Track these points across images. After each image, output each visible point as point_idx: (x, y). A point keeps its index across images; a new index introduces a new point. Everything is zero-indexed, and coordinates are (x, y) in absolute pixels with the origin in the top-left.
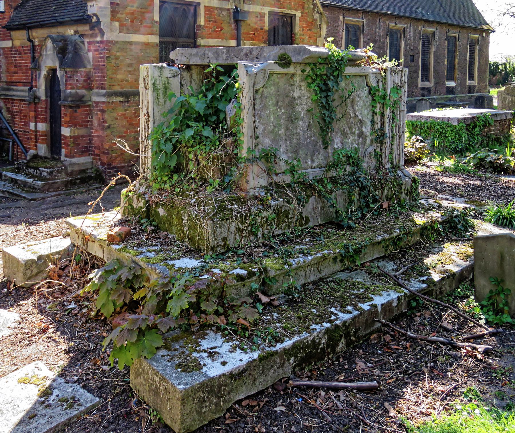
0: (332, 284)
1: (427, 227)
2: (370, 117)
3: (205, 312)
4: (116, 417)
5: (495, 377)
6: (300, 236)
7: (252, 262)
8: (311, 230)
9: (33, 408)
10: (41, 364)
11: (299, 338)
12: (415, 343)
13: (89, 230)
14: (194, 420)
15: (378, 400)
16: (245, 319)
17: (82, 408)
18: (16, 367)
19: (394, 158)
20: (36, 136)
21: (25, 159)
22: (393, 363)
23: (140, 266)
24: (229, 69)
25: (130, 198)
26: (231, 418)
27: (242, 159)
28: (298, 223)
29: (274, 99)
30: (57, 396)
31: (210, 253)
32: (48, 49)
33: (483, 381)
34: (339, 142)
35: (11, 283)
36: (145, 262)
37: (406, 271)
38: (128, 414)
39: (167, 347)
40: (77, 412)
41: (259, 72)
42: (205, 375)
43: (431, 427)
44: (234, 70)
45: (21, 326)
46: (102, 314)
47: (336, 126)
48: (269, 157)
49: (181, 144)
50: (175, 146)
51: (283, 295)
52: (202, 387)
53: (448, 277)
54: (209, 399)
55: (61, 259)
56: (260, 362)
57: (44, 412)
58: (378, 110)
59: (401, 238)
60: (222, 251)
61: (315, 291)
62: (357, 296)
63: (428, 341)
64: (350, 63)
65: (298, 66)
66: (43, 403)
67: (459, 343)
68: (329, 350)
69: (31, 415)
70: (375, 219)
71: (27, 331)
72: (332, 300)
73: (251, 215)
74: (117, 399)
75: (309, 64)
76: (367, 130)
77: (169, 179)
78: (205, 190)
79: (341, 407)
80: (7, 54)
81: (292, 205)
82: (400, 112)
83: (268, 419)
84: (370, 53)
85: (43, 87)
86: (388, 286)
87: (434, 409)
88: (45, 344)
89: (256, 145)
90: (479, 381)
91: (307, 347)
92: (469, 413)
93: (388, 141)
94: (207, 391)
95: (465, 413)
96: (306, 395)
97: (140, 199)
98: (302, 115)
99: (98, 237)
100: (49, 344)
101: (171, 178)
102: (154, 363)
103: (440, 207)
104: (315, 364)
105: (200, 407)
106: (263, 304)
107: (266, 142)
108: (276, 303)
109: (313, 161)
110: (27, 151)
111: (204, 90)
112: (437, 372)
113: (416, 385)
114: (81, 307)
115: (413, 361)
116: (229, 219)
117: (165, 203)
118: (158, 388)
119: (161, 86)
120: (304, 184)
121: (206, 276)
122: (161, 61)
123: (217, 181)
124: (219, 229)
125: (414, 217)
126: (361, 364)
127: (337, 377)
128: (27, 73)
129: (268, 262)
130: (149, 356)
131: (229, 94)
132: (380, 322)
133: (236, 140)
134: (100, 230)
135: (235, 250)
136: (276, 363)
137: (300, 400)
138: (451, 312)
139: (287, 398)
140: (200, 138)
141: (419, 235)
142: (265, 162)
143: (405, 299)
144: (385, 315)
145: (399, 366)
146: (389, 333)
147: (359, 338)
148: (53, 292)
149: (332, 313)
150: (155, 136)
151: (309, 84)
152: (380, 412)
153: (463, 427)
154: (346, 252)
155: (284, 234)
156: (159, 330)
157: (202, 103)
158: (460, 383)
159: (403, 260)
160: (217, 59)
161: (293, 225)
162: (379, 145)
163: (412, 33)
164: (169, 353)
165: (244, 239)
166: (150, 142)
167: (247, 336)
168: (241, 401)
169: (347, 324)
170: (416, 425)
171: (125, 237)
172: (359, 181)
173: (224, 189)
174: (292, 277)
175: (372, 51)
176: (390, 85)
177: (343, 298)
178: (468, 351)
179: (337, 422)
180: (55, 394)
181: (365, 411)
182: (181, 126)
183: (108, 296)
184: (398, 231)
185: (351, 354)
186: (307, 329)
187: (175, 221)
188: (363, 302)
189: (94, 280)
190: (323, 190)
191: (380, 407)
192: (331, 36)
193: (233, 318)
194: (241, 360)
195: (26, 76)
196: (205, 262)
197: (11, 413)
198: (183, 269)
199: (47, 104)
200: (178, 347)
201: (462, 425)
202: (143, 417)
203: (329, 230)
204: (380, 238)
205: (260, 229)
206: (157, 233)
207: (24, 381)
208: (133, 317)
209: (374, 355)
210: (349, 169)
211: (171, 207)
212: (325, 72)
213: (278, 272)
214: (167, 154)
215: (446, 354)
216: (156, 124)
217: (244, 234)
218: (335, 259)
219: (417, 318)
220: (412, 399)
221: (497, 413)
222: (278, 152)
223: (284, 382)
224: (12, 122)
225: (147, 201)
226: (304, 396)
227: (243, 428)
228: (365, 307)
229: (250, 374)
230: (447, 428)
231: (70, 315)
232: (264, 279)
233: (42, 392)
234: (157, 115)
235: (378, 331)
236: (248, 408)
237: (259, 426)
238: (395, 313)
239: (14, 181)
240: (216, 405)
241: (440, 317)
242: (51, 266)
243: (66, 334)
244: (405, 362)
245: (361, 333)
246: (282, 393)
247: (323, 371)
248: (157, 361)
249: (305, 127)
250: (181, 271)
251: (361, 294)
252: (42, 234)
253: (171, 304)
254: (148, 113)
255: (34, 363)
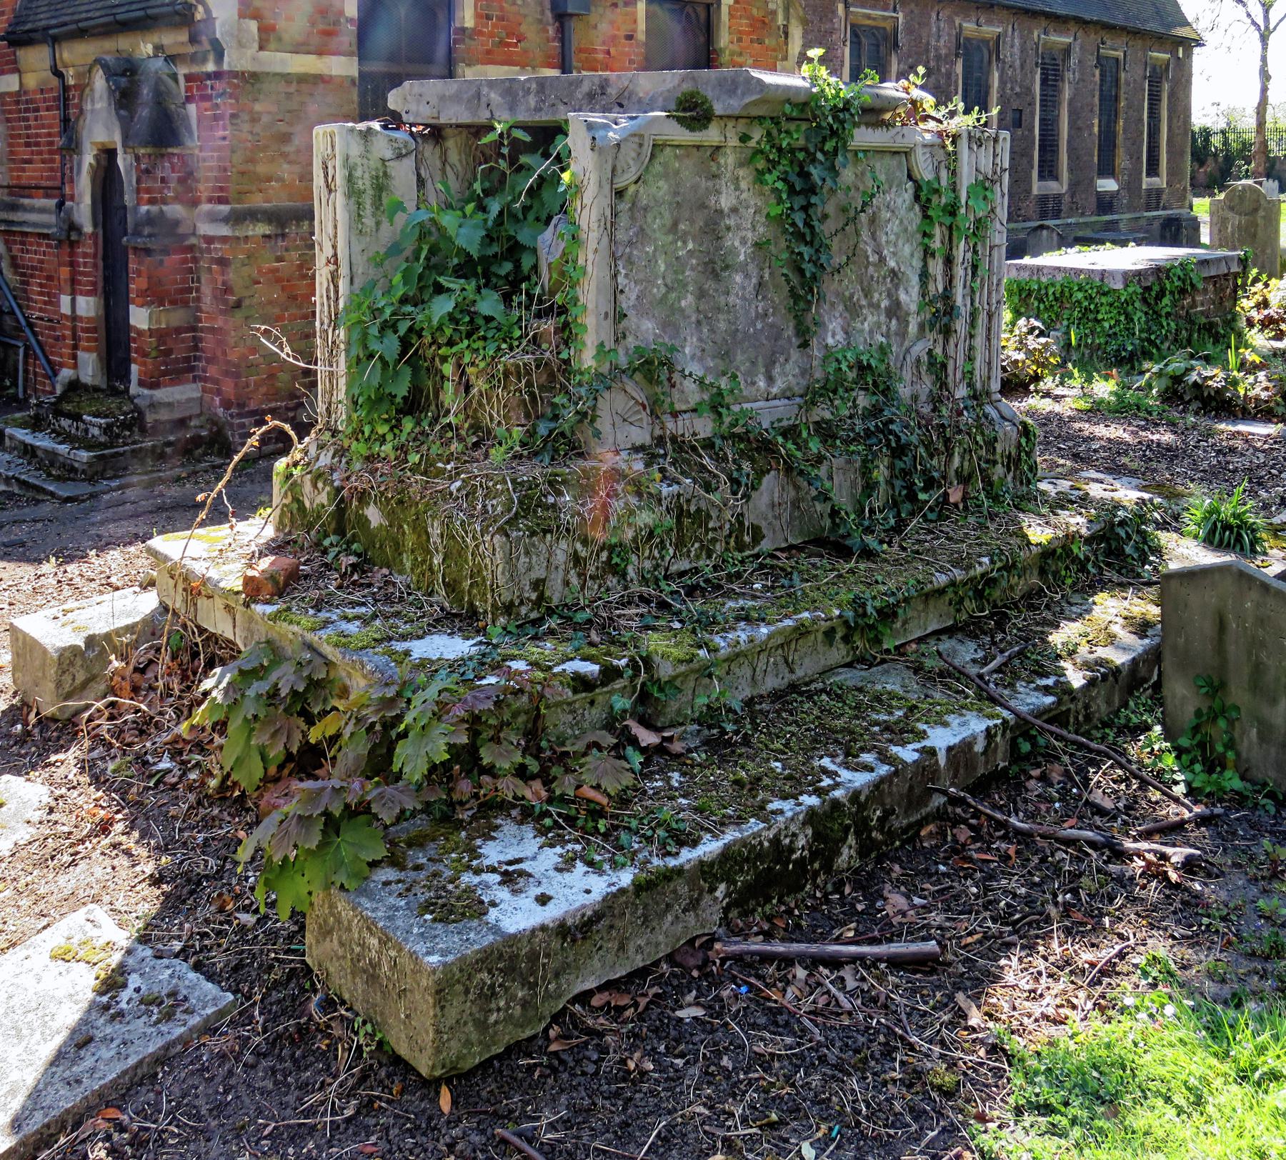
0: (824, 697)
1: (1054, 551)
2: (917, 263)
3: (490, 771)
4: (275, 1040)
5: (1208, 926)
6: (738, 575)
7: (613, 642)
8: (768, 561)
9: (84, 1022)
10: (99, 913)
11: (738, 835)
12: (1027, 845)
13: (199, 568)
14: (468, 1043)
15: (939, 987)
16: (597, 787)
17: (194, 1020)
18: (46, 919)
19: (977, 372)
20: (74, 329)
21: (52, 393)
22: (977, 897)
23: (324, 657)
24: (546, 136)
25: (294, 484)
26: (564, 1037)
27: (582, 374)
28: (732, 541)
29: (667, 215)
30: (137, 990)
31: (502, 620)
32: (97, 95)
33: (1183, 937)
34: (839, 330)
35: (30, 708)
36: (336, 645)
37: (1005, 664)
38: (303, 1032)
39: (395, 861)
40: (182, 1029)
41: (625, 140)
42: (495, 929)
43: (1067, 1052)
44: (559, 137)
45: (53, 817)
46: (235, 784)
47: (830, 286)
48: (653, 369)
49: (420, 336)
50: (405, 344)
51: (696, 727)
52: (487, 959)
53: (1104, 677)
54: (507, 989)
55: (135, 645)
56: (638, 896)
57: (109, 1030)
58: (936, 244)
59: (994, 580)
60: (534, 615)
61: (779, 716)
62: (887, 728)
63: (1058, 840)
64: (868, 118)
65: (730, 124)
66: (106, 1008)
67: (1129, 844)
68: (816, 865)
69: (79, 1038)
70: (930, 532)
71: (66, 829)
72: (822, 739)
73: (607, 519)
74: (275, 995)
75: (761, 119)
76: (910, 297)
77: (391, 429)
78: (487, 456)
79: (848, 1006)
80: (10, 112)
81: (718, 495)
82: (991, 248)
83: (660, 1039)
84: (916, 93)
85: (87, 200)
86: (962, 701)
87: (1074, 1007)
88: (108, 862)
89: (620, 338)
90: (1174, 938)
91: (760, 856)
92: (1151, 1016)
93: (960, 326)
94: (501, 970)
95: (1143, 1016)
96: (759, 977)
97: (320, 485)
98: (742, 258)
99: (222, 585)
100: (116, 862)
101: (396, 427)
102: (363, 900)
103: (1085, 500)
104: (780, 902)
105: (481, 1009)
106: (643, 750)
107: (646, 329)
108: (677, 747)
109: (770, 379)
110: (54, 370)
111: (479, 191)
112: (1080, 915)
113: (1031, 948)
114: (185, 767)
115: (1023, 890)
116: (551, 531)
117: (382, 493)
118: (375, 965)
119: (368, 183)
120: (749, 440)
121: (492, 680)
122: (363, 118)
123: (518, 432)
124: (523, 559)
125: (1025, 525)
126: (896, 901)
127: (837, 932)
128: (53, 161)
129: (655, 643)
130: (351, 885)
131: (546, 203)
132: (945, 793)
133: (566, 325)
134: (225, 568)
135: (566, 612)
136: (678, 897)
137: (744, 989)
138: (1111, 767)
139: (709, 987)
140: (472, 321)
141: (1036, 572)
142: (643, 382)
143: (1003, 735)
144: (955, 776)
145: (990, 902)
146: (965, 822)
147: (891, 835)
148: (122, 731)
149: (825, 771)
150: (354, 317)
151: (760, 173)
152: (946, 1018)
153: (1140, 1051)
154: (857, 615)
155: (696, 571)
156: (375, 816)
157: (476, 227)
158: (1132, 942)
159: (999, 637)
160: (512, 108)
161: (719, 547)
162: (941, 337)
163: (1016, 50)
164: (402, 875)
165: (589, 583)
166: (342, 333)
167: (602, 830)
168: (589, 994)
169: (862, 798)
170: (1033, 1047)
171: (286, 584)
172: (891, 432)
173: (536, 454)
174: (720, 680)
175: (922, 87)
176: (966, 178)
177: (852, 732)
178: (1149, 864)
179: (838, 1044)
180: (132, 986)
181: (909, 1015)
182: (421, 289)
183: (249, 738)
184: (986, 560)
185: (871, 875)
186: (760, 811)
187: (410, 540)
188: (903, 743)
189: (214, 694)
190: (799, 454)
191: (946, 1005)
192: (820, 45)
193: (565, 785)
194: (588, 892)
195: (52, 170)
196: (488, 644)
197: (38, 1036)
198: (431, 662)
199: (96, 244)
200: (424, 861)
201: (1136, 1045)
202: (340, 1039)
203: (813, 560)
204: (942, 579)
205: (634, 558)
206: (364, 572)
207: (63, 956)
208: (309, 784)
209: (931, 876)
210: (863, 401)
211: (398, 505)
212: (802, 142)
213: (683, 668)
214: (385, 364)
215: (1099, 871)
216: (357, 285)
217: (591, 570)
218: (829, 634)
219: (1032, 784)
220: (1022, 984)
221: (1213, 1012)
222: (679, 356)
223: (701, 946)
224: (22, 296)
225: (339, 490)
226: (753, 980)
227: (595, 1062)
228: (908, 754)
229: (612, 927)
230: (1103, 1053)
231: (162, 787)
232: (643, 684)
233: (104, 982)
234: (360, 261)
235: (940, 815)
236: (608, 1012)
237: (637, 1055)
238: (981, 771)
239: (28, 451)
240: (525, 1004)
241: (1086, 780)
242: (116, 664)
243: (152, 836)
244: (1006, 892)
245: (898, 822)
246: (695, 973)
247: (800, 917)
248: (370, 896)
249: (750, 288)
250: (428, 667)
251: (896, 723)
252: (93, 585)
253: (403, 752)
254: (335, 255)
255: (84, 910)
